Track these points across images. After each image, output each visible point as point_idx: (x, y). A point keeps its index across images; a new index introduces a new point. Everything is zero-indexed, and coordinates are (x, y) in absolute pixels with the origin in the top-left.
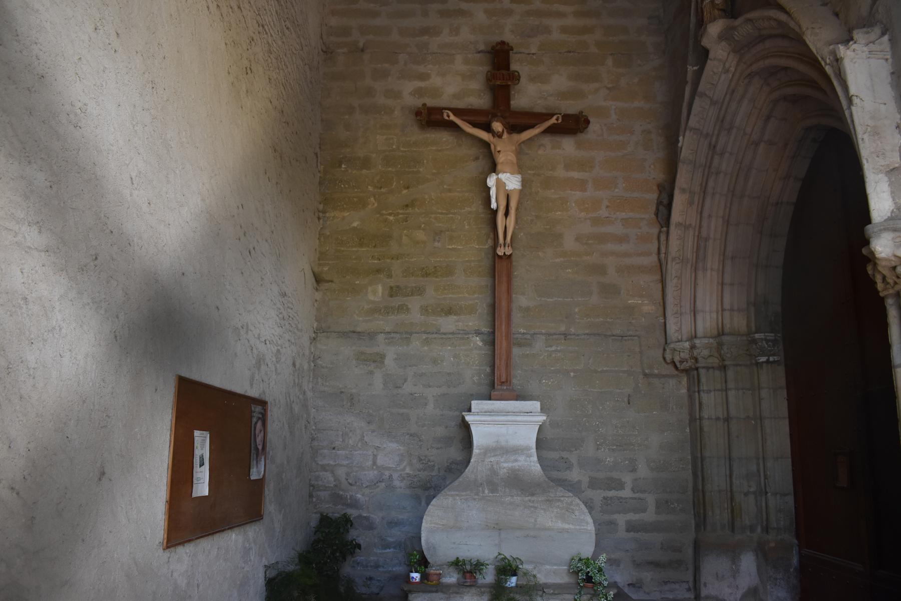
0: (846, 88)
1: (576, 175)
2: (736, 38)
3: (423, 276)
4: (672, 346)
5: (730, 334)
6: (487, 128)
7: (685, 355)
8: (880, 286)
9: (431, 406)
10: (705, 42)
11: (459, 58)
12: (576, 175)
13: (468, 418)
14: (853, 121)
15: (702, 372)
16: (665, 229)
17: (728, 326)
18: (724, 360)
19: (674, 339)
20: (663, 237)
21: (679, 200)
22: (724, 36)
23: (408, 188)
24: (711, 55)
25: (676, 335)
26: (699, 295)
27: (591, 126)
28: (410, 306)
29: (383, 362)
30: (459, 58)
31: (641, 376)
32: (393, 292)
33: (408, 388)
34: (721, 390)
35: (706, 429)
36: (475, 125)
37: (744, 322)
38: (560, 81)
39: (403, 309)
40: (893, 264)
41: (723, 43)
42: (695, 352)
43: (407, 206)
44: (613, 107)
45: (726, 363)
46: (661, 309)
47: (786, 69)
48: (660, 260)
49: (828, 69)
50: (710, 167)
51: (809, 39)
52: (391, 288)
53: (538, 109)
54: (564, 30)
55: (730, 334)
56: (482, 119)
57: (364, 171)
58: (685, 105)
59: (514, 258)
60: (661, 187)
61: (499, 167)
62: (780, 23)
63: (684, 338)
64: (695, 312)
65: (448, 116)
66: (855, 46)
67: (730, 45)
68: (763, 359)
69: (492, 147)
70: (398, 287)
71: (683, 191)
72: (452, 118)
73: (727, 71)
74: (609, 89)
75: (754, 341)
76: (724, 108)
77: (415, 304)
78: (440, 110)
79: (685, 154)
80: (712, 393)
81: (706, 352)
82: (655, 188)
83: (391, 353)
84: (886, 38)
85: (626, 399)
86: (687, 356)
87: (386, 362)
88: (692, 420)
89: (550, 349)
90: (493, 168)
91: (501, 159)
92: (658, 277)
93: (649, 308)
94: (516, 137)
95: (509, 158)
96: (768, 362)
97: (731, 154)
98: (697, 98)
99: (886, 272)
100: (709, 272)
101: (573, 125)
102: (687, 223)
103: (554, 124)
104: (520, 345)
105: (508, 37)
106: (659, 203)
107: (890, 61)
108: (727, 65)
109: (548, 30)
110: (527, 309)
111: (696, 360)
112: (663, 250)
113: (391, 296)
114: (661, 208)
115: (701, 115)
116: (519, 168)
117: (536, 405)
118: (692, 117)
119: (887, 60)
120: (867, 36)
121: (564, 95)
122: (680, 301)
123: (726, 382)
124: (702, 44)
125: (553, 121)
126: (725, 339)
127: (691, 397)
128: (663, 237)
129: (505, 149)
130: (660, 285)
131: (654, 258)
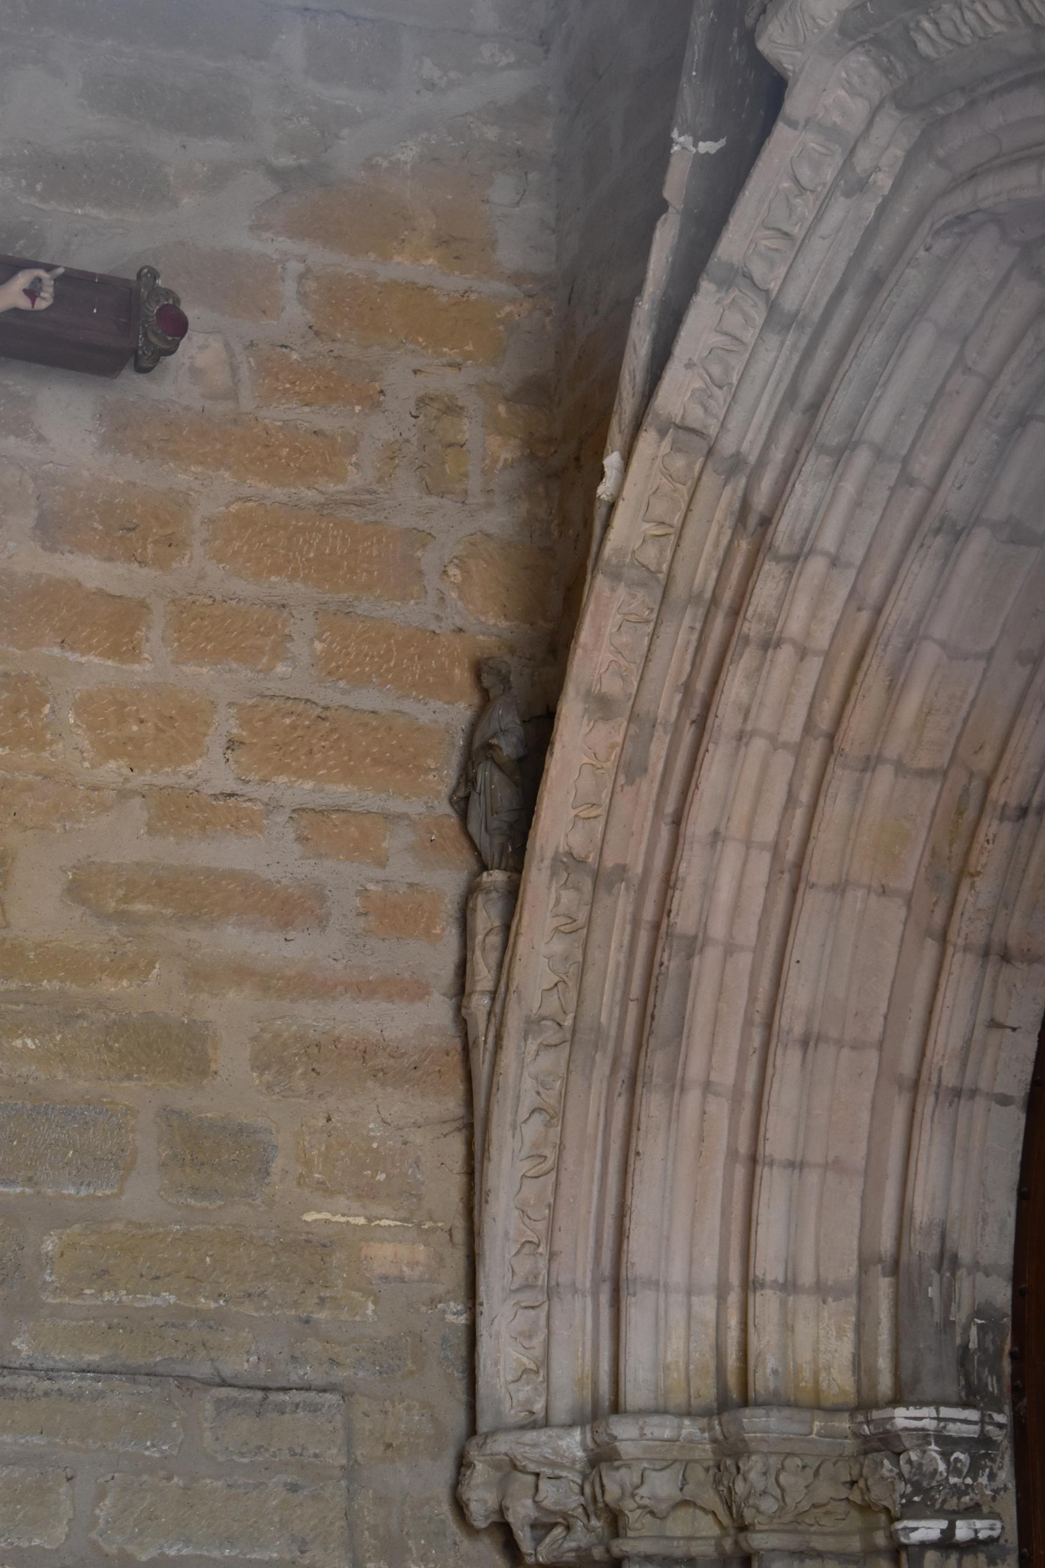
1: (91, 571)
2: (923, 46)
4: (502, 1445)
5: (777, 1401)
7: (561, 1494)
10: (776, 42)
12: (91, 571)
16: (497, 877)
17: (771, 1362)
18: (743, 1528)
19: (513, 1414)
20: (486, 917)
21: (578, 744)
24: (795, 104)
25: (524, 1392)
26: (644, 1206)
27: (187, 347)
37: (845, 1348)
44: (295, 267)
45: (758, 1541)
46: (457, 1258)
48: (462, 1023)
50: (736, 612)
55: (777, 1401)
63: (563, 1406)
64: (617, 1288)
67: (887, 71)
68: (928, 1530)
71: (602, 706)
74: (277, 175)
75: (888, 1443)
76: (824, 354)
79: (625, 534)
81: (662, 1486)
82: (461, 675)
86: (573, 1502)
92: (452, 1105)
93: (401, 1252)
96: (946, 1543)
97: (834, 562)
98: (706, 286)
100: (693, 1098)
102: (609, 863)
103: (16, 311)
106: (476, 753)
108: (864, 158)
111: (616, 1522)
112: (483, 975)
118: (674, 372)
122: (551, 1229)
124: (762, 45)
126: (758, 1423)
128: (486, 917)
130: (457, 1146)
131: (438, 1011)
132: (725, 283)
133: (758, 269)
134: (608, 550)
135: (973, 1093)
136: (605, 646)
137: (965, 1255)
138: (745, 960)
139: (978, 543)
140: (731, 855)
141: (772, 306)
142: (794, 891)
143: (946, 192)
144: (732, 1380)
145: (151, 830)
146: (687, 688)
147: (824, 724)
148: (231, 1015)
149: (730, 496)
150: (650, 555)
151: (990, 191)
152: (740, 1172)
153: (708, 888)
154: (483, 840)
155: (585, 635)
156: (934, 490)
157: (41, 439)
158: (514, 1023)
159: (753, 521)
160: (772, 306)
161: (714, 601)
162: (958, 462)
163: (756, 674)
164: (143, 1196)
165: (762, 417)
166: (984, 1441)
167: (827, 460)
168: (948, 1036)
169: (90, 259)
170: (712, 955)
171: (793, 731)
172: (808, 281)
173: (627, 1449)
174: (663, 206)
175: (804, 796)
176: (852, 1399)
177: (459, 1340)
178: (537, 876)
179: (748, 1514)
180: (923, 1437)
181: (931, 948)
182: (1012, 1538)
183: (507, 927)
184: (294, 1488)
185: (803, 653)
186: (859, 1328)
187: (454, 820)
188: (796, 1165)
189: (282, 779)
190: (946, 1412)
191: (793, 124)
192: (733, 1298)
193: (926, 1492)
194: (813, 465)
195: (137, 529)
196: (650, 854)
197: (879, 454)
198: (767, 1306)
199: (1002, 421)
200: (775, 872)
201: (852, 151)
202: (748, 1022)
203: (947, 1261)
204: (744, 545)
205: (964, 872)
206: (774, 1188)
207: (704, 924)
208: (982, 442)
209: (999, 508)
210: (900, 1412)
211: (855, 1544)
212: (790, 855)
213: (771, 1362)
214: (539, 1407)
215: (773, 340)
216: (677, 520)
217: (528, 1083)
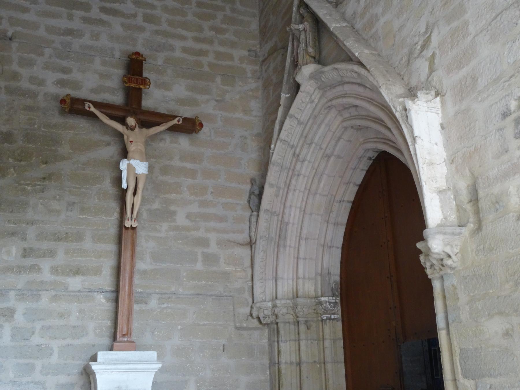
0: (412, 132)
1: (188, 165)
2: (323, 79)
3: (55, 241)
6: (122, 121)
7: (268, 312)
8: (428, 271)
9: (55, 356)
10: (298, 79)
11: (98, 61)
12: (188, 165)
13: (95, 367)
14: (416, 154)
15: (281, 326)
16: (255, 213)
17: (301, 290)
18: (297, 317)
22: (313, 77)
23: (46, 163)
24: (302, 89)
25: (261, 296)
28: (41, 266)
29: (13, 317)
30: (98, 61)
31: (233, 329)
32: (26, 253)
33: (36, 340)
34: (295, 340)
35: (283, 371)
36: (112, 117)
37: (313, 288)
38: (180, 90)
39: (35, 268)
40: (442, 257)
41: (312, 81)
42: (276, 311)
43: (44, 178)
44: (220, 115)
47: (356, 106)
49: (398, 115)
50: (293, 170)
51: (384, 92)
52: (25, 250)
53: (162, 110)
54: (185, 50)
56: (120, 114)
57: (6, 145)
58: (277, 121)
59: (138, 230)
60: (253, 181)
61: (130, 155)
62: (359, 75)
63: (268, 298)
65: (89, 108)
66: (418, 102)
67: (317, 83)
69: (125, 137)
70: (31, 249)
71: (272, 185)
72: (93, 109)
73: (312, 102)
75: (320, 303)
77: (46, 265)
78: (82, 101)
79: (275, 158)
80: (288, 343)
81: (284, 311)
82: (249, 181)
83: (21, 308)
84: (438, 98)
85: (221, 348)
86: (270, 313)
87: (16, 316)
88: (272, 364)
89: (162, 306)
90: (125, 154)
91: (132, 148)
94: (144, 130)
95: (139, 147)
97: (309, 162)
98: (288, 118)
99: (435, 262)
100: (288, 248)
101: (190, 126)
102: (273, 210)
103: (176, 124)
104: (137, 302)
105: (140, 48)
106: (251, 193)
107: (440, 115)
108: (313, 97)
109: (172, 48)
110: (145, 272)
111: (277, 316)
113: (24, 257)
114: (253, 196)
115: (290, 131)
116: (147, 157)
117: (153, 354)
118: (283, 131)
119: (438, 114)
120: (426, 96)
121: (182, 102)
122: (265, 269)
123: (299, 334)
124: (296, 79)
125: (175, 121)
127: (271, 345)
128: (254, 220)
129: (136, 139)
132: (291, 117)
133: (296, 115)
134: (272, 160)
135: (333, 247)
136: (273, 175)
137: (332, 273)
138: (296, 226)
139: (332, 158)
140: (293, 209)
141: (299, 121)
142: (304, 214)
143: (327, 103)
144: (295, 294)
145: (199, 207)
146: (285, 182)
147: (308, 188)
148: (213, 237)
149: (292, 151)
150: (279, 161)
151: (334, 102)
152: (296, 260)
153: (290, 215)
154: (252, 207)
155: (269, 174)
156: (325, 150)
157: (180, 144)
158: (258, 237)
159: (296, 155)
160: (299, 121)
161: (290, 169)
162: (329, 146)
163: (297, 180)
164: (199, 266)
165: (297, 139)
166: (336, 302)
167: (308, 146)
168: (329, 238)
169: (188, 115)
170: (290, 225)
171: (303, 189)
172: (304, 117)
173: (278, 305)
174: (280, 105)
175: (305, 199)
176: (314, 296)
177: (251, 287)
178: (262, 213)
179: (298, 315)
180: (326, 302)
181: (326, 224)
182: (341, 318)
183: (257, 222)
184: (225, 312)
185: (304, 177)
186: (315, 284)
187: (248, 204)
188: (305, 259)
189: (220, 198)
190: (330, 298)
191: (302, 92)
192: (295, 280)
193: (327, 311)
194: (306, 146)
195: (195, 158)
196: (280, 209)
197: (316, 144)
198: (300, 282)
199: (336, 139)
200: (300, 212)
201: (311, 97)
202: (296, 236)
203: (329, 274)
204: (294, 159)
205: (331, 211)
206: (301, 262)
207: (289, 220)
208: (333, 142)
209: (335, 153)
210: (322, 298)
211: (315, 319)
212: (303, 209)
213: (301, 290)
214: (264, 298)
215: (299, 126)
216: (283, 155)
217: (261, 246)
